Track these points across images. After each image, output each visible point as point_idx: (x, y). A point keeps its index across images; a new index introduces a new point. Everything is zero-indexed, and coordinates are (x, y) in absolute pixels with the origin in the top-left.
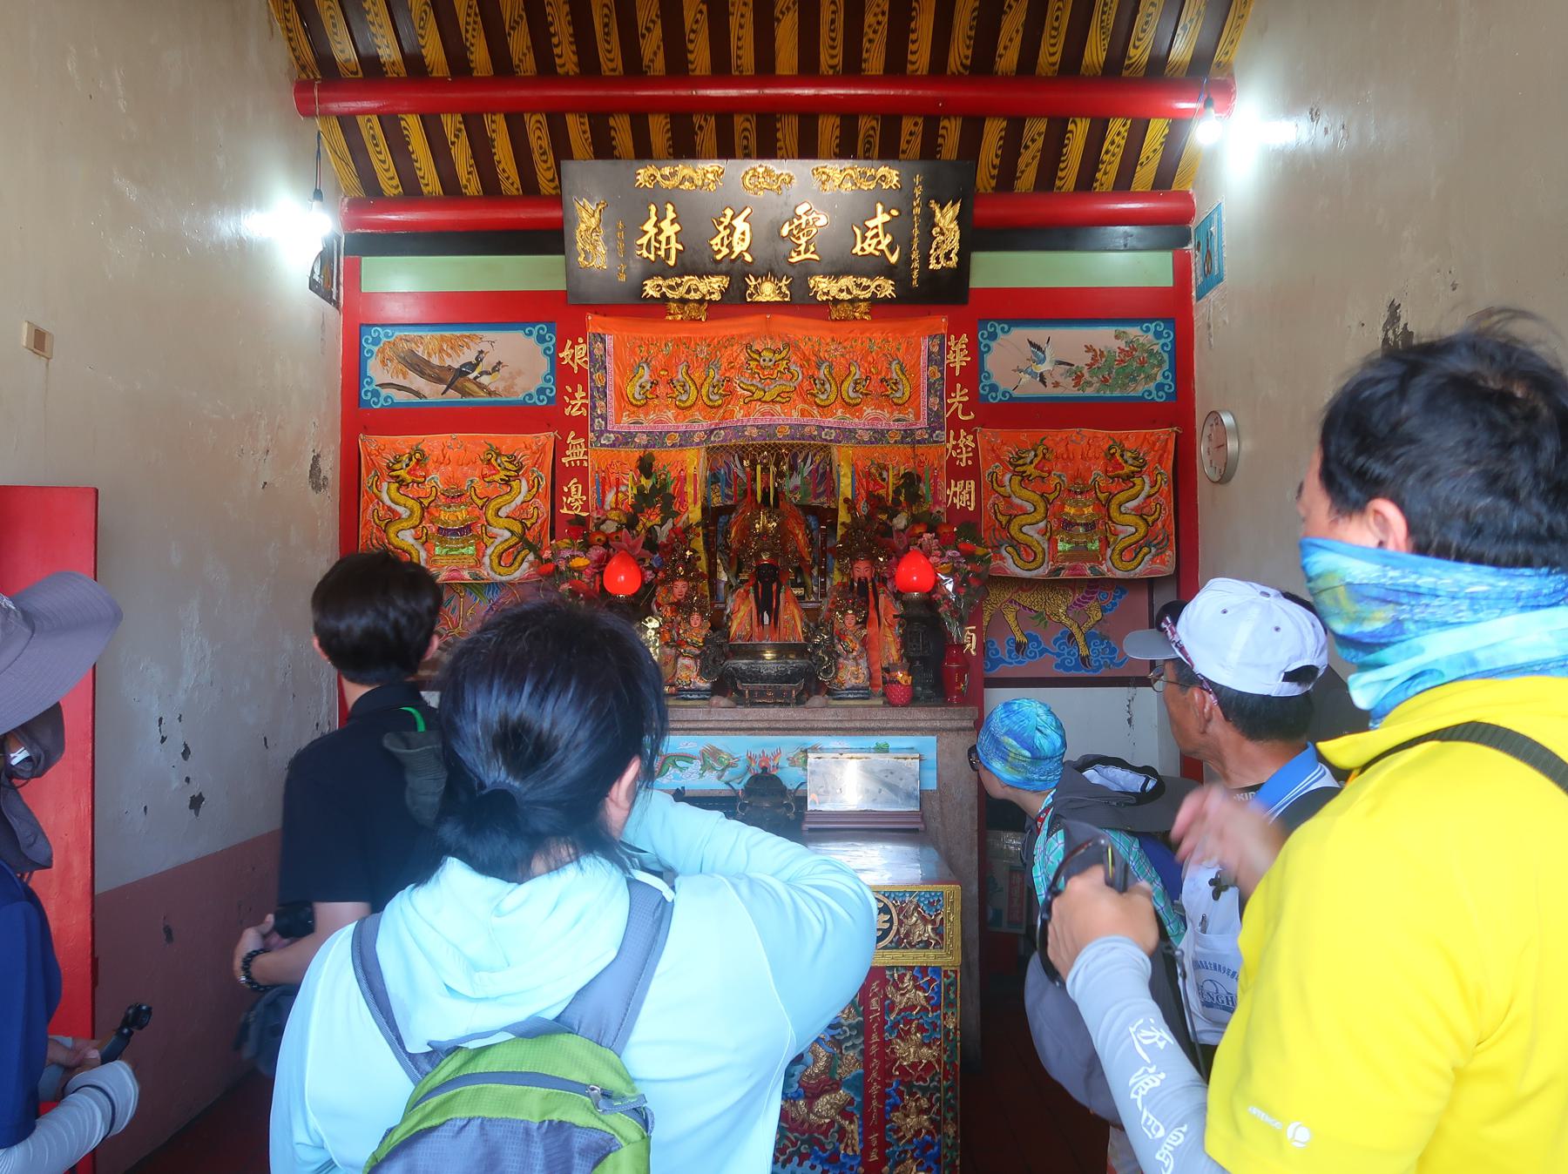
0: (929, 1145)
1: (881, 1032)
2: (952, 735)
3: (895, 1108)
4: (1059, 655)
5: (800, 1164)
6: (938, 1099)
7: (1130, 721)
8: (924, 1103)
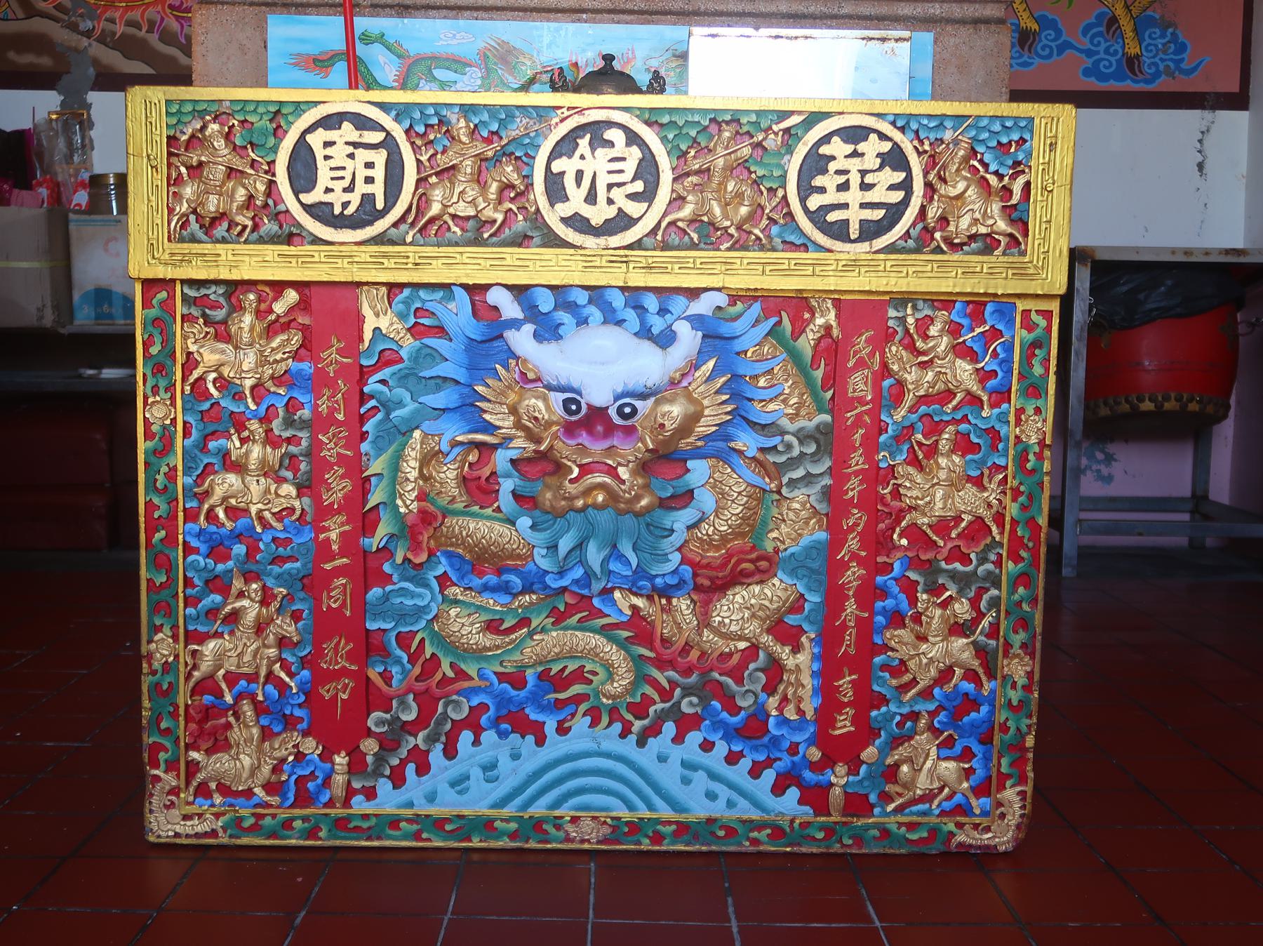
0: (971, 703)
1: (871, 446)
2: (965, 32)
3: (897, 619)
4: (1089, 53)
5: (678, 739)
6: (995, 603)
7: (1200, 166)
8: (962, 609)
